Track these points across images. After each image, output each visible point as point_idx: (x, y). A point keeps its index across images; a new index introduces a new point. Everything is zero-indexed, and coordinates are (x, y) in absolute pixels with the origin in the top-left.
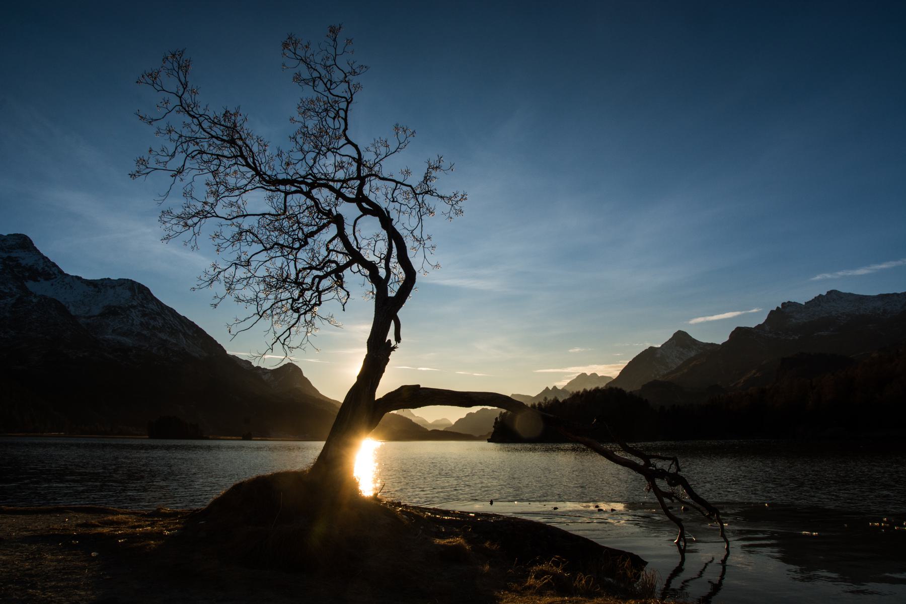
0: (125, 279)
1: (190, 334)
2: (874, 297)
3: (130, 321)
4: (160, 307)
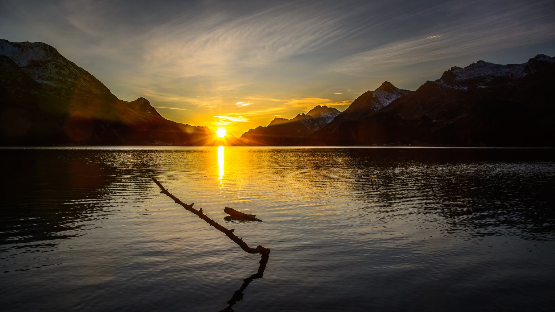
1: (87, 79)
2: (505, 66)
4: (65, 61)
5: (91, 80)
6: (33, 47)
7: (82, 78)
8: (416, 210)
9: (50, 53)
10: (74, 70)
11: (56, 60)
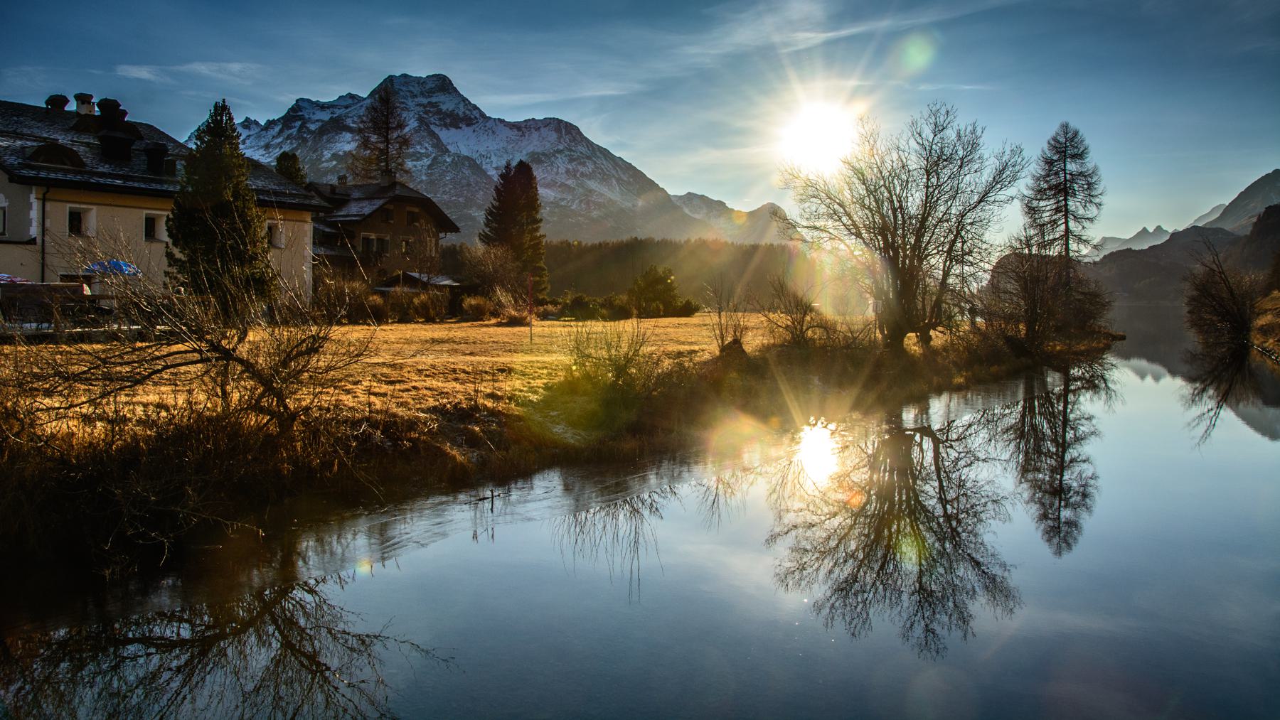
0: (550, 119)
1: (625, 179)
3: (555, 170)
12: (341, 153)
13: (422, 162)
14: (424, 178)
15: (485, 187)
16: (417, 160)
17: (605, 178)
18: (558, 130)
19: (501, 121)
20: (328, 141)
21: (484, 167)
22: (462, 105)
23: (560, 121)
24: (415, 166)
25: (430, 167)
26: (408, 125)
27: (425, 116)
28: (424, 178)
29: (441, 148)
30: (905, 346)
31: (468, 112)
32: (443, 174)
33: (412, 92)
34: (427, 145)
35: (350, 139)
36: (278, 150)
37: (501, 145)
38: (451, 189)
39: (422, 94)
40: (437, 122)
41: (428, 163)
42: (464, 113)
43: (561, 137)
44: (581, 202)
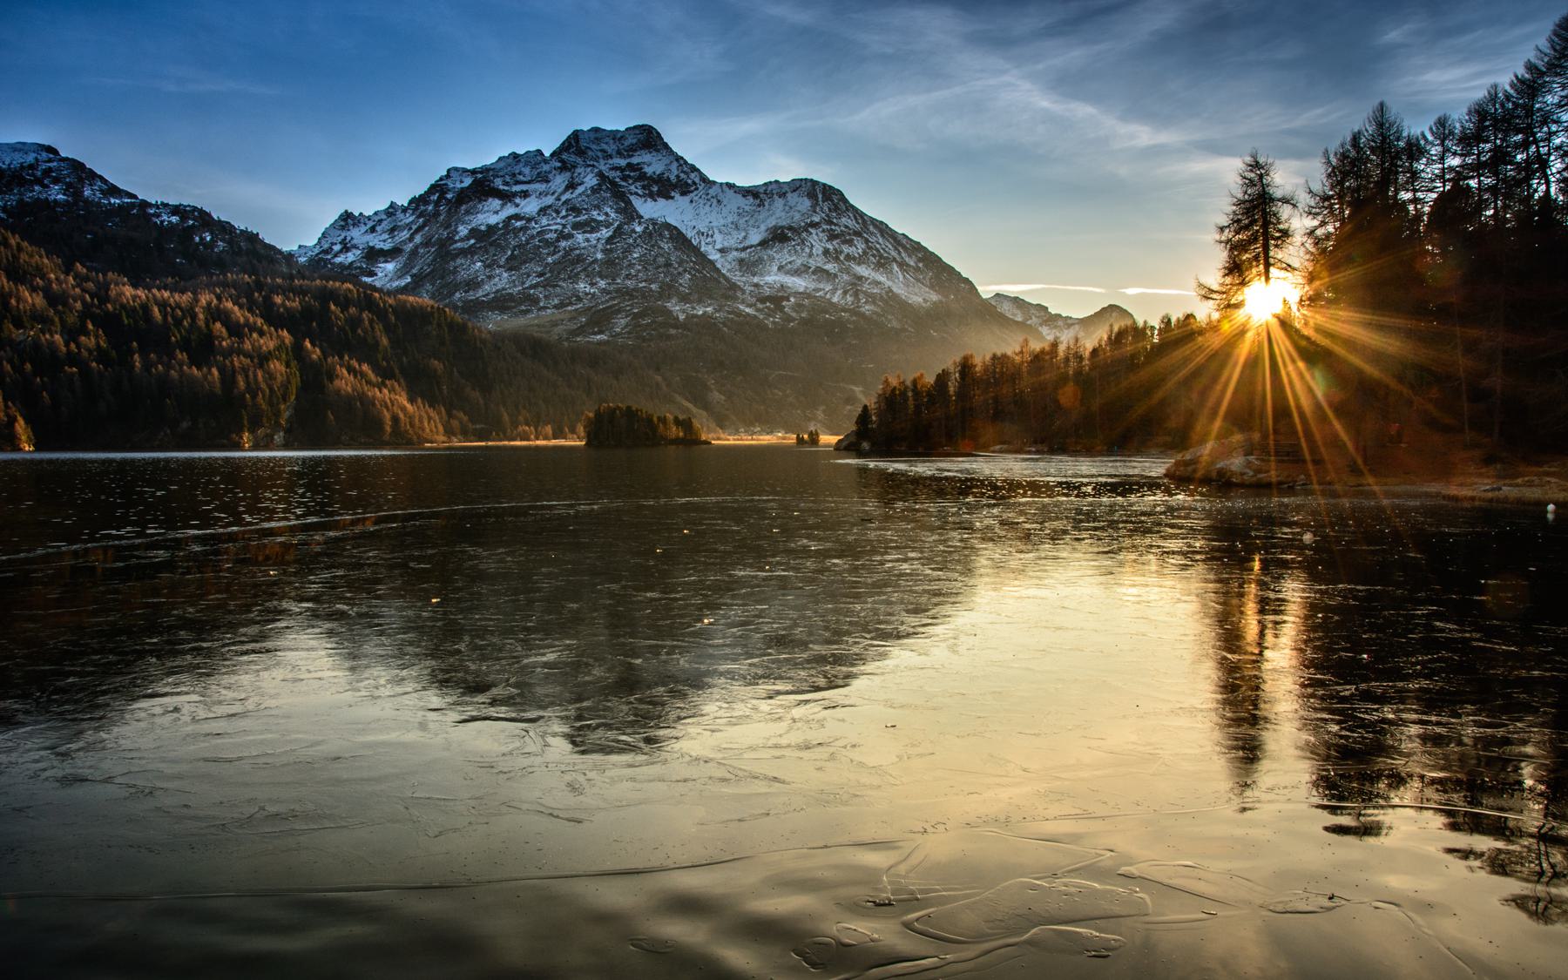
0: (801, 180)
1: (912, 263)
3: (807, 250)
5: (921, 265)
6: (786, 192)
7: (896, 262)
8: (1090, 572)
9: (823, 202)
10: (878, 243)
11: (835, 221)
12: (483, 228)
13: (599, 235)
14: (599, 256)
15: (694, 269)
16: (591, 232)
17: (882, 263)
18: (812, 195)
19: (730, 186)
20: (468, 212)
21: (702, 249)
22: (675, 164)
23: (814, 183)
24: (588, 240)
25: (609, 240)
26: (582, 183)
27: (624, 184)
28: (599, 256)
29: (631, 214)
30: (490, 200)
31: (682, 176)
32: (628, 250)
33: (603, 151)
34: (608, 210)
35: (498, 208)
36: (405, 232)
37: (730, 219)
38: (639, 271)
39: (619, 153)
40: (640, 192)
41: (607, 235)
42: (678, 176)
43: (817, 204)
44: (845, 293)
